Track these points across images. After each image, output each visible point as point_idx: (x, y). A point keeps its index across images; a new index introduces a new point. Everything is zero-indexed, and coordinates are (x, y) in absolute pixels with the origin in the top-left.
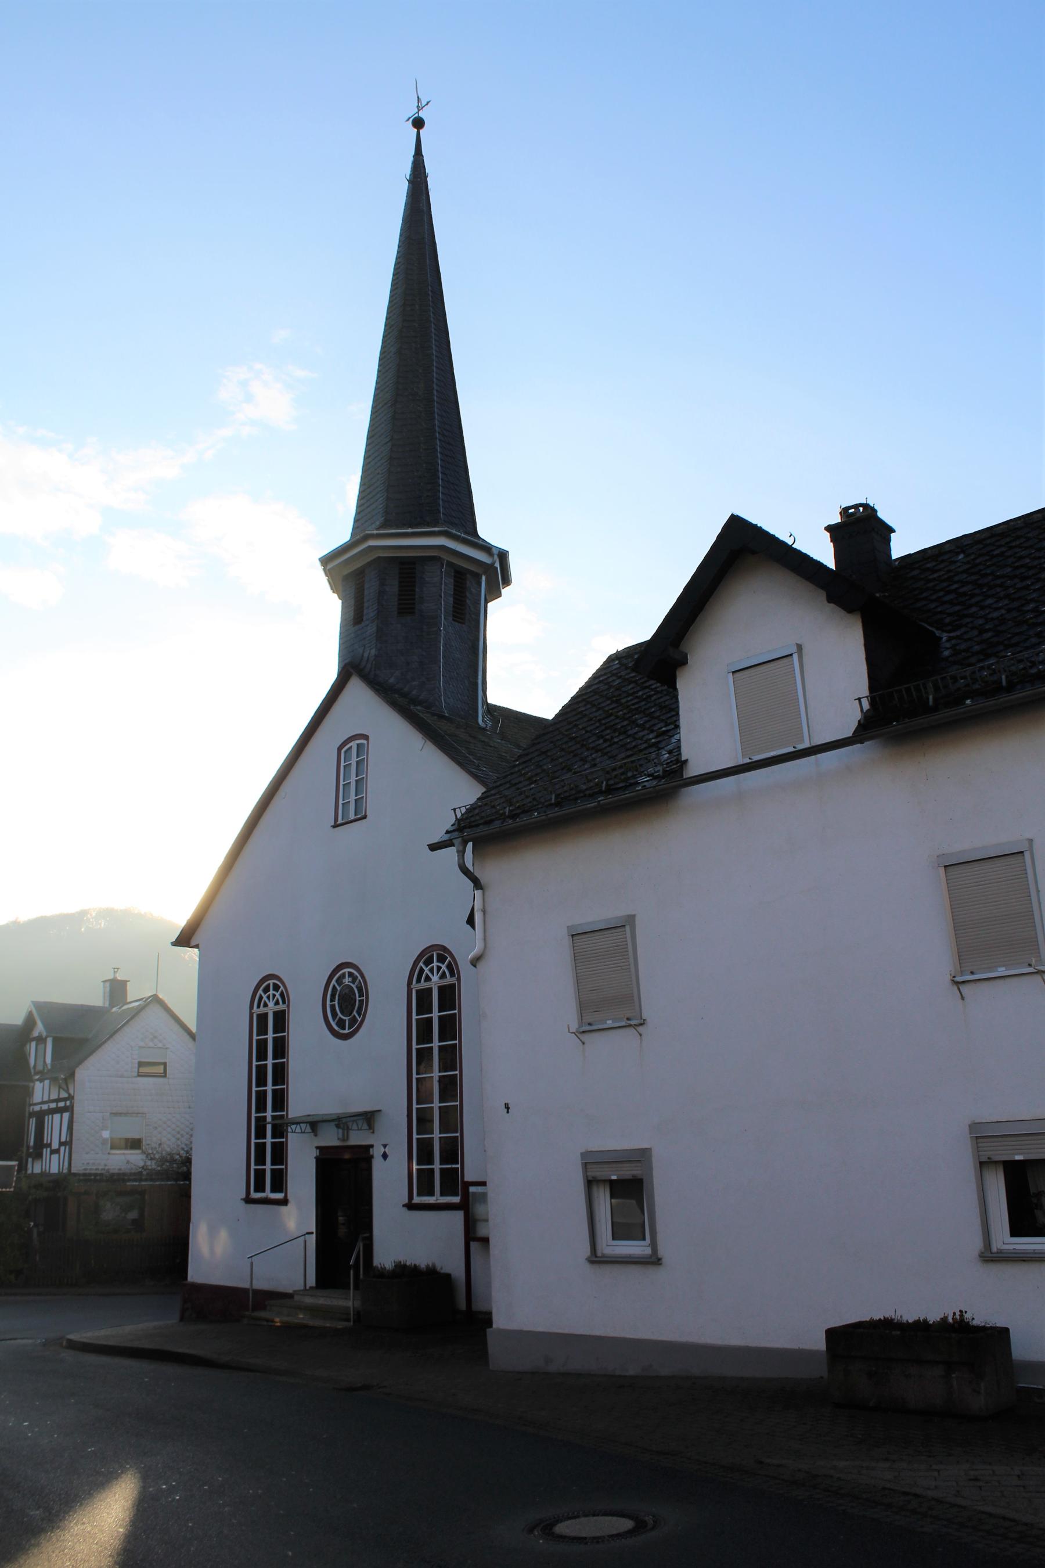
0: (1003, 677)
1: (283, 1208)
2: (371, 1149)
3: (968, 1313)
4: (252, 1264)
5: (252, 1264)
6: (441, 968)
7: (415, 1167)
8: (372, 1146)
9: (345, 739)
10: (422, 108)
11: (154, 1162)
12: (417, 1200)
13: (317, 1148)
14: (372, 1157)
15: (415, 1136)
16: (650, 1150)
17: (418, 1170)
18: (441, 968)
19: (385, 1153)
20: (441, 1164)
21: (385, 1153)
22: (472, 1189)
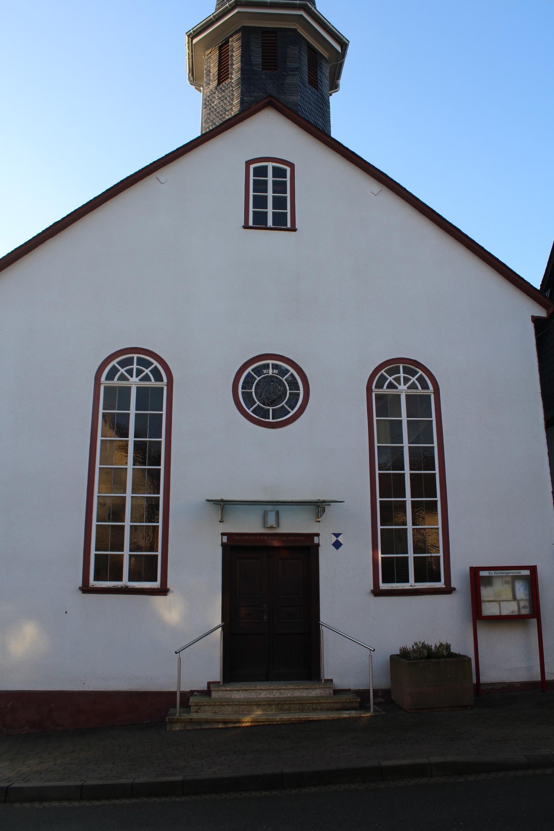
0: (431, 467)
1: (158, 600)
2: (316, 539)
3: (65, 612)
4: (180, 659)
5: (180, 659)
6: (390, 383)
7: (380, 556)
8: (318, 535)
9: (254, 158)
10: (207, 114)
11: (250, 723)
12: (383, 586)
13: (223, 534)
14: (318, 545)
15: (379, 527)
16: (536, 566)
17: (382, 558)
18: (390, 383)
19: (337, 541)
20: (414, 553)
21: (337, 541)
22: (483, 573)
